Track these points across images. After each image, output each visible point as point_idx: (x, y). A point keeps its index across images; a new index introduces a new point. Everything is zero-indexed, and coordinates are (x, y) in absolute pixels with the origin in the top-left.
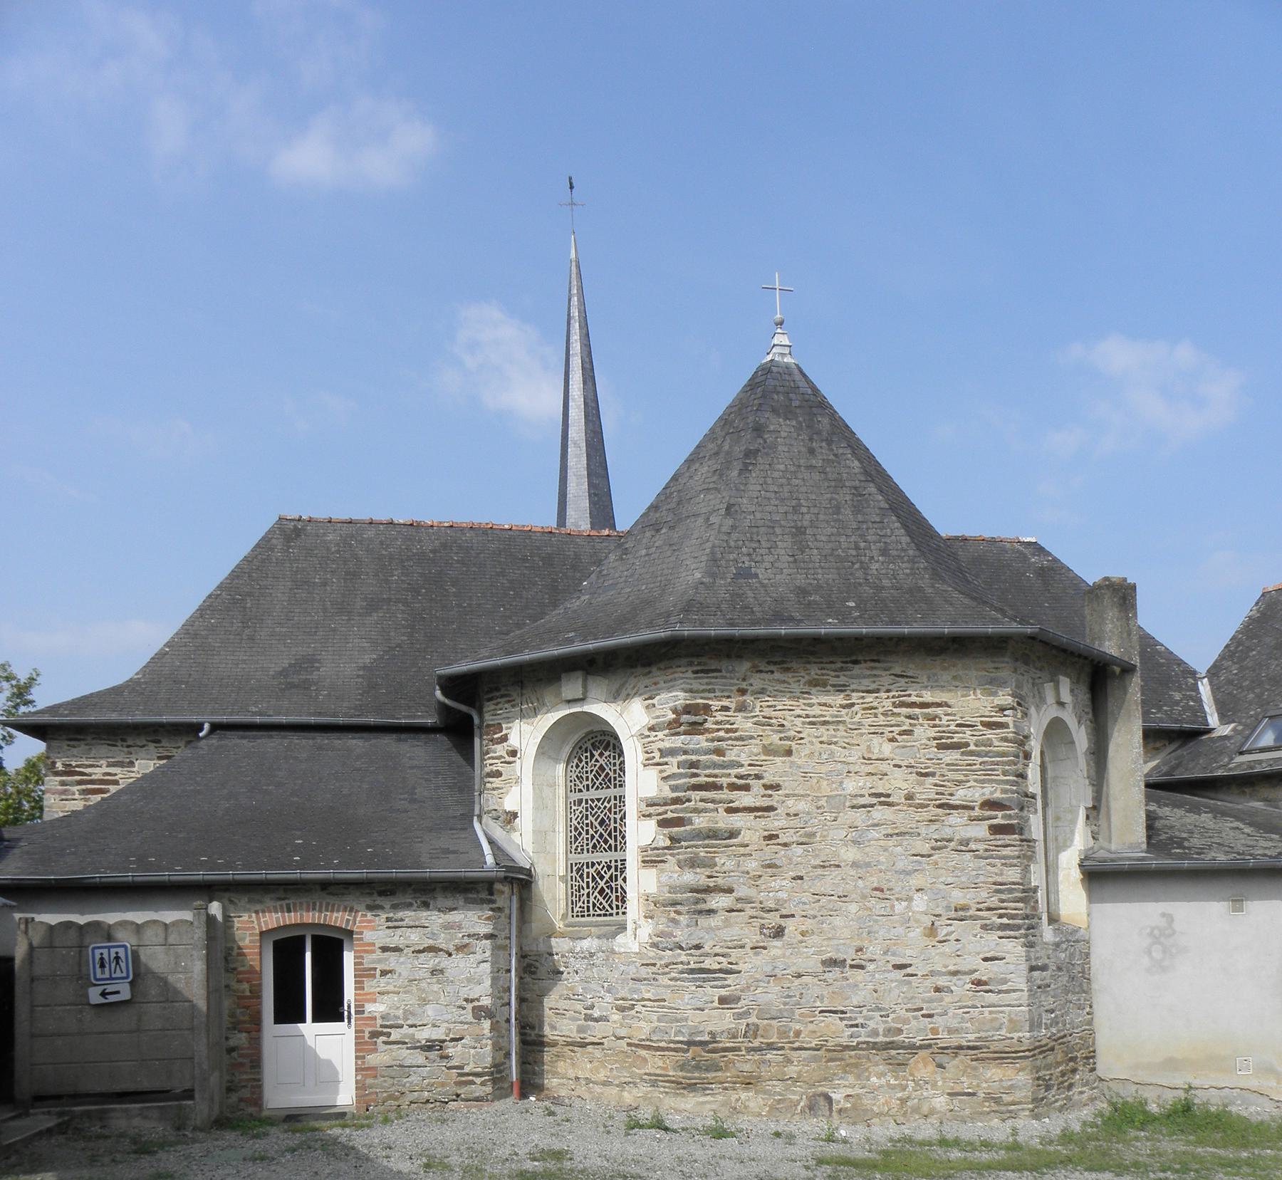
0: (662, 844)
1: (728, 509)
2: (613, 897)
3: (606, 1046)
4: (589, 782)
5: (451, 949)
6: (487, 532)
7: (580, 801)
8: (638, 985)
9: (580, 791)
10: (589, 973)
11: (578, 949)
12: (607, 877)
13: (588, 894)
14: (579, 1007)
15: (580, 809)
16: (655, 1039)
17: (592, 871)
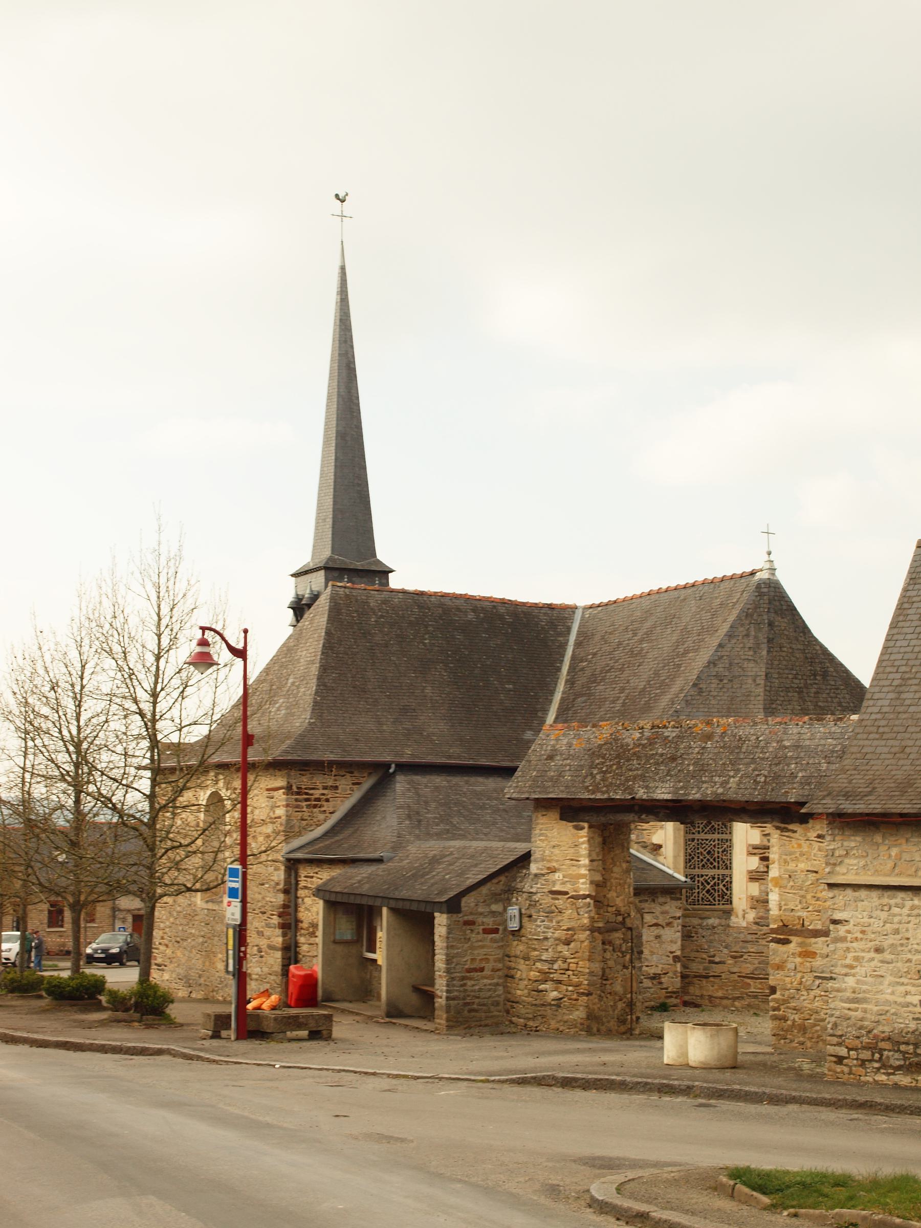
0: (762, 870)
1: (766, 676)
2: (716, 895)
3: (723, 977)
4: (700, 829)
5: (664, 925)
6: (467, 599)
7: (693, 840)
8: (746, 945)
9: (693, 833)
10: (712, 938)
11: (705, 924)
12: (712, 883)
13: (698, 893)
14: (705, 956)
15: (693, 844)
16: (756, 973)
17: (701, 879)
